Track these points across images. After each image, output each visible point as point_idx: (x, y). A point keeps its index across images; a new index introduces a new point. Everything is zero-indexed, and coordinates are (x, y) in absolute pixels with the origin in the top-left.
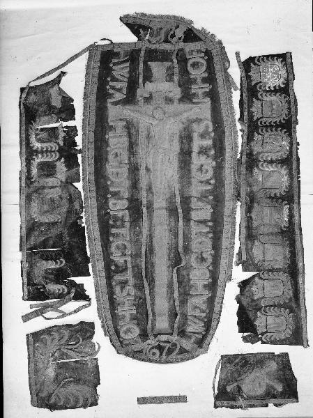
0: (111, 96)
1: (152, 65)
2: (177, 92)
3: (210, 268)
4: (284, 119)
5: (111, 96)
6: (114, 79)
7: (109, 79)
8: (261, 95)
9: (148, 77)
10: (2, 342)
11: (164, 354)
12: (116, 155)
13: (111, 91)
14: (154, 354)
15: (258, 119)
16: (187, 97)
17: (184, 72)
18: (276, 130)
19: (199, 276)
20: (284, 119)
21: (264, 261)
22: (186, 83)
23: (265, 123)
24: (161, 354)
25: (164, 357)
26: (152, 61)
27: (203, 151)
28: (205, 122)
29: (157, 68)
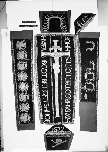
0: (42, 49)
1: (54, 41)
2: (61, 49)
3: (71, 98)
4: (21, 104)
5: (42, 49)
6: (69, 113)
7: (41, 45)
8: (27, 111)
9: (53, 44)
10: (1, 134)
11: (59, 130)
12: (16, 34)
13: (69, 110)
14: (56, 131)
15: (28, 104)
16: (64, 50)
17: (63, 43)
18: (22, 101)
19: (68, 101)
20: (21, 104)
21: (24, 63)
22: (64, 46)
23: (26, 103)
24: (58, 130)
25: (59, 131)
26: (59, 118)
27: (68, 65)
28: (69, 57)
29: (56, 42)
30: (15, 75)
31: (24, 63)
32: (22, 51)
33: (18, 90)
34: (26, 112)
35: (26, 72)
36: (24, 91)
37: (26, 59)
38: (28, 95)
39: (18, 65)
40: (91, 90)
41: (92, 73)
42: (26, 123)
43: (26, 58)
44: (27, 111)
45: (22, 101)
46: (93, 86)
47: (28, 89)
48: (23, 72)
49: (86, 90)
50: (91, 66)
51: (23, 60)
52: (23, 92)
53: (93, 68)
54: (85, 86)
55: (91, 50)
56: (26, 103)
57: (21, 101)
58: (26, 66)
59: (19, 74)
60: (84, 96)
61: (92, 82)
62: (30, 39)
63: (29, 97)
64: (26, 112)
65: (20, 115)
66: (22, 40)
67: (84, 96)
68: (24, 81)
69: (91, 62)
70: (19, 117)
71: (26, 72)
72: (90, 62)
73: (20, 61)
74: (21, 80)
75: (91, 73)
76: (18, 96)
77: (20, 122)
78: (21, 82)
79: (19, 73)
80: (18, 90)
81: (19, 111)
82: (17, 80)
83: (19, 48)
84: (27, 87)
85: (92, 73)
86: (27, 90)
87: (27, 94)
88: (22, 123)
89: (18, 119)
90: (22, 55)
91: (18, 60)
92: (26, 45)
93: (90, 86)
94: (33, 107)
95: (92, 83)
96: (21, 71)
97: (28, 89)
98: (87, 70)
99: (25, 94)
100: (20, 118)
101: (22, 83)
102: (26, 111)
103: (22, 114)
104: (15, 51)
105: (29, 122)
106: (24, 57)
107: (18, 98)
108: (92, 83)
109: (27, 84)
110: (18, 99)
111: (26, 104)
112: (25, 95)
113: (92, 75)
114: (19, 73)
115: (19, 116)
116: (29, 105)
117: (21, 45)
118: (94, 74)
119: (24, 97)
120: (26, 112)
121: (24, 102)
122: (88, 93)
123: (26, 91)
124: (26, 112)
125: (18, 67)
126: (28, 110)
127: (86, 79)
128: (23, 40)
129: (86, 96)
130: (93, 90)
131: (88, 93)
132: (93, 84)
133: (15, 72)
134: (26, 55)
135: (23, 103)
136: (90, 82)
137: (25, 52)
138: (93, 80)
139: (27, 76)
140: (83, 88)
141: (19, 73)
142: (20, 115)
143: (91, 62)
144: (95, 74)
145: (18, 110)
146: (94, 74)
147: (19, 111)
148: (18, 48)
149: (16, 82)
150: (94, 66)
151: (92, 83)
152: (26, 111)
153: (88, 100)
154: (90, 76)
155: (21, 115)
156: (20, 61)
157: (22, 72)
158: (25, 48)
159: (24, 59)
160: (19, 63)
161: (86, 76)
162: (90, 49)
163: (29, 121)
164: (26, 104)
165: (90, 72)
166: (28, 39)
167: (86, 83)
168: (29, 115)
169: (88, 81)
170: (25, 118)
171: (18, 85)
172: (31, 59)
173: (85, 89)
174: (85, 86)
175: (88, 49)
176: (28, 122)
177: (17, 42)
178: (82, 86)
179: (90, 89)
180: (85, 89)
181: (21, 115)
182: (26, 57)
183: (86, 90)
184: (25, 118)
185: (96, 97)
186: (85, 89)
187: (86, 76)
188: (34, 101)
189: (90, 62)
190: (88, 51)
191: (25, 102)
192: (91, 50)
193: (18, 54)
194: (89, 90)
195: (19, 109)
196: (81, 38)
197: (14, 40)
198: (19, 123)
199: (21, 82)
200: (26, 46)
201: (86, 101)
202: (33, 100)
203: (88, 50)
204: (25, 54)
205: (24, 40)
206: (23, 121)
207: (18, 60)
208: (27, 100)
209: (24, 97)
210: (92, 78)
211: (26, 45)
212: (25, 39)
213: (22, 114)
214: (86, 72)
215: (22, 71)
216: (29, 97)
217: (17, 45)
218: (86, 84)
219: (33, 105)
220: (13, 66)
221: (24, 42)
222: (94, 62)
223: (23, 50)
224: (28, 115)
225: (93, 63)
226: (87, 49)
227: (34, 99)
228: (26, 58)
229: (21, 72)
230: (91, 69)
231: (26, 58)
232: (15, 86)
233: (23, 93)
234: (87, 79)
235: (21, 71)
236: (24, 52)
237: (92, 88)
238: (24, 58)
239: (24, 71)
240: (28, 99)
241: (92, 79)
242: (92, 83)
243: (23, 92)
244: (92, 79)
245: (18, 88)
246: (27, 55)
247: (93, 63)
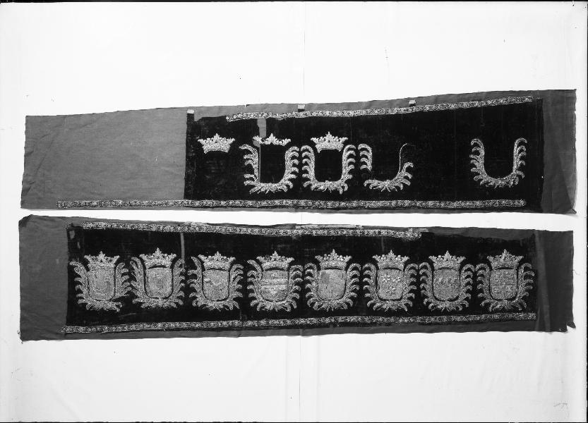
4: (428, 303)
8: (469, 269)
15: (431, 263)
18: (411, 291)
21: (203, 269)
30: (263, 322)
31: (199, 269)
32: (132, 278)
33: (350, 311)
34: (475, 273)
35: (251, 262)
36: (355, 276)
37: (182, 261)
38: (382, 260)
39: (212, 305)
40: (250, 170)
41: (346, 176)
42: (535, 278)
43: (173, 256)
44: (469, 269)
45: (411, 291)
46: (277, 180)
47: (348, 258)
48: (252, 276)
49: (251, 143)
50: (385, 168)
51: (187, 277)
52: (361, 284)
53: (374, 183)
54: (272, 139)
55: (473, 170)
56: (424, 274)
57: (410, 299)
58: (216, 261)
59: (259, 301)
60: (217, 137)
61: (299, 180)
62: (68, 231)
63: (391, 254)
64: (475, 273)
65: (485, 310)
66: (72, 274)
67: (217, 137)
68: (303, 278)
69: (408, 170)
70: (496, 316)
71: (251, 262)
72: (406, 165)
73: (188, 289)
74: (296, 291)
75: (346, 168)
76: (381, 312)
77: (524, 311)
78: (303, 290)
79: (254, 298)
80: (350, 311)
81: (465, 311)
82: (294, 314)
83: (118, 295)
84: (333, 264)
85: (346, 176)
86: (349, 263)
87: (375, 262)
88: (531, 301)
89: (506, 321)
90: (159, 278)
91: (181, 303)
92: (102, 256)
93: (272, 163)
94: (449, 233)
95: (288, 176)
96: (245, 291)
97: (348, 258)
98: (361, 146)
99: (372, 274)
100: (503, 310)
101: (309, 290)
102: (468, 277)
103: (480, 295)
104: (129, 318)
105: (530, 262)
106: (168, 271)
107: (390, 313)
108: (293, 176)
109: (317, 262)
110: (399, 313)
111: (429, 273)
112: (381, 273)
113: (336, 176)
114: (255, 301)
115: (493, 313)
116: (433, 258)
117: (101, 279)
118: (340, 185)
119: (391, 280)
120: (475, 276)
121: (417, 281)
122: (235, 156)
123: (355, 268)
124: (475, 276)
125: (220, 305)
126: (463, 264)
127: (313, 145)
128: (71, 270)
129: (217, 144)
130: (252, 183)
131: (235, 156)
132: (285, 182)
133: (250, 323)
134: (159, 257)
135: (419, 290)
136: (294, 165)
137: (143, 261)
138: (305, 185)
139: (275, 260)
140: (263, 131)
141: (254, 298)
142: (485, 310)
143: (408, 170)
144: (341, 192)
145: (458, 319)
146: (340, 185)
147: (465, 311)
148: (116, 301)
149: (302, 321)
150: (387, 184)
151: (293, 176)
152: (468, 277)
153: (195, 157)
154: (328, 164)
155: (488, 305)
156: (188, 289)
157: (251, 283)
158: (116, 264)
159: (178, 271)
160: (201, 301)
161: (328, 142)
162: (482, 161)
163: (521, 263)
164: (429, 273)
165: (352, 167)
166: (72, 244)
167: (289, 146)
168: (491, 259)
169: (300, 153)
170: (504, 279)
171: (322, 313)
172: (178, 235)
173: (258, 139)
174: (272, 139)
175: (483, 153)
176: (526, 269)
177: (80, 301)
178: (271, 122)
179: (255, 166)
180: (258, 139)
181: (488, 305)
182: (167, 260)
183: (251, 143)
184: (504, 279)
185: (215, 202)
186: (258, 140)
187: (328, 142)
188: (415, 229)
189: (406, 165)
190: (467, 151)
191: (418, 277)
192: (473, 170)
193: (147, 305)
194: (254, 160)
195: (455, 312)
196: (540, 110)
197: (70, 322)
198: (531, 315)
199: (303, 290)
200: (109, 254)
201: (193, 146)
202: (409, 235)
203: (477, 153)
204: (149, 260)
205: (73, 263)
206: (522, 291)
207: (181, 303)
208: (406, 264)
209: (391, 280)
210: (320, 177)
211: (102, 256)
212: (71, 260)
213: (480, 295)
214: (354, 140)
215: (244, 282)
216: (391, 254)
217: (99, 305)
218: (286, 141)
219: (436, 232)
220: (218, 332)
221: (85, 263)
222: (408, 183)
223: (129, 274)
224: (489, 264)
225: (402, 177)
226: (479, 142)
227: (405, 230)
228: (174, 261)
229: (252, 291)
230: (369, 167)
231: (173, 256)
232: (327, 326)
233: (367, 283)
234: (315, 150)
235: (245, 291)
236: (138, 270)
237: (264, 179)
238: (172, 267)
239: (245, 275)
240: (400, 261)
241: (312, 174)
242: (288, 176)
243: (361, 284)
244: (312, 174)
245: (338, 312)
246: (158, 252)
247: (402, 177)
